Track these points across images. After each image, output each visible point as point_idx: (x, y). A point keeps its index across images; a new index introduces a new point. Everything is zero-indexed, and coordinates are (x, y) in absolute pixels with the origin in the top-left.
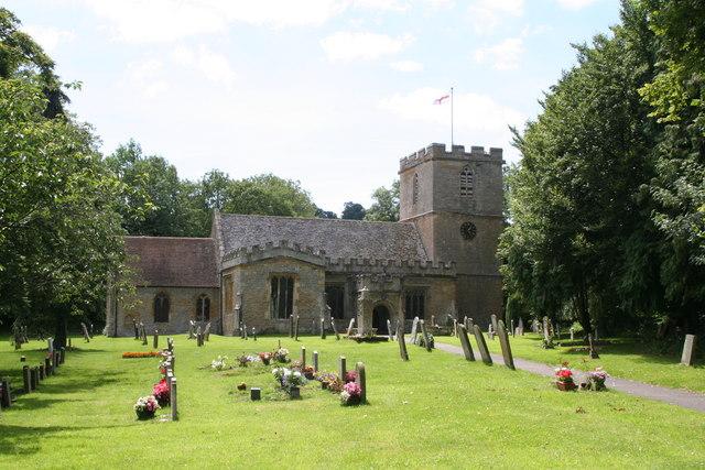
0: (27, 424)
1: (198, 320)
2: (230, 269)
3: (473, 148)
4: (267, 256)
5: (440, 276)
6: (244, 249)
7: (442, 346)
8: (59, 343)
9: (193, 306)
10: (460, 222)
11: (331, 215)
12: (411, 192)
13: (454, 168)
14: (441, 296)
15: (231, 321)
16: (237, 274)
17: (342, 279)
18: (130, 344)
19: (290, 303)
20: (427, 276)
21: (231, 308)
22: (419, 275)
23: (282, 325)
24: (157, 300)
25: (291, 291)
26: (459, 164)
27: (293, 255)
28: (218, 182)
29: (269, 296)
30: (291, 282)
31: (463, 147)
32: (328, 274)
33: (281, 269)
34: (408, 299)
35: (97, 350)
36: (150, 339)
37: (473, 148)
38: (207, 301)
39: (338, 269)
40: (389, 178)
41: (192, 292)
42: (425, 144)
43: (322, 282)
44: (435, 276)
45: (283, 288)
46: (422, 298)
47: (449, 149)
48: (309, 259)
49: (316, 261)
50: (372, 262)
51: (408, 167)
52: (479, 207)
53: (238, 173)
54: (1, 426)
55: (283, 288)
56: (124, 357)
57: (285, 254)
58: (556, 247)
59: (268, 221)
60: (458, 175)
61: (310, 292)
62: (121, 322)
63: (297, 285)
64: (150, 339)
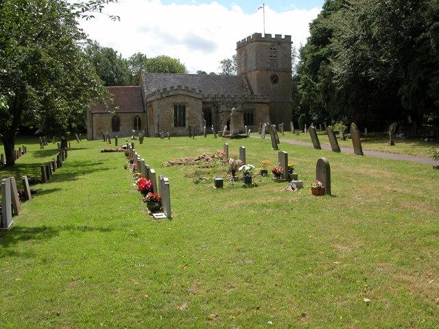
0: (44, 189)
1: (136, 129)
2: (151, 101)
3: (285, 36)
4: (171, 94)
5: (261, 103)
6: (158, 91)
7: (284, 141)
8: (64, 146)
9: (132, 122)
10: (270, 74)
11: (195, 75)
12: (243, 59)
13: (266, 46)
14: (262, 111)
15: (89, 135)
16: (155, 105)
17: (211, 105)
18: (101, 144)
19: (184, 119)
20: (255, 103)
21: (153, 122)
22: (250, 102)
23: (180, 130)
24: (113, 120)
25: (184, 112)
26: (269, 44)
27: (184, 93)
28: (140, 59)
29: (173, 116)
30: (184, 108)
31: (271, 35)
32: (203, 102)
33: (179, 100)
34: (245, 115)
35: (82, 151)
36: (113, 141)
37: (285, 36)
38: (139, 119)
39: (208, 100)
40: (231, 52)
41: (132, 115)
42: (250, 33)
43: (201, 107)
44: (259, 103)
45: (180, 110)
46: (252, 114)
47: (273, 36)
48: (193, 95)
49: (198, 96)
50: (226, 96)
51: (241, 46)
52: (280, 67)
53: (150, 55)
54: (415, 131)
55: (180, 110)
56: (102, 152)
57: (181, 92)
58: (356, 80)
59: (169, 77)
60: (264, 50)
61: (195, 112)
62: (95, 132)
63: (187, 109)
64: (113, 141)
